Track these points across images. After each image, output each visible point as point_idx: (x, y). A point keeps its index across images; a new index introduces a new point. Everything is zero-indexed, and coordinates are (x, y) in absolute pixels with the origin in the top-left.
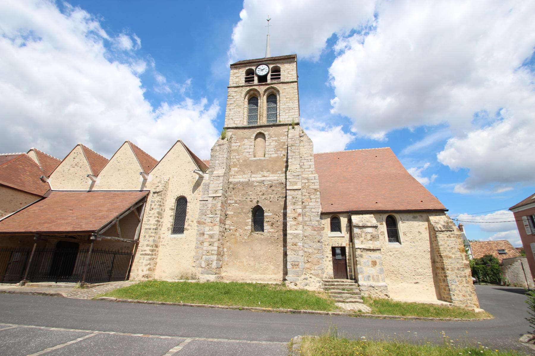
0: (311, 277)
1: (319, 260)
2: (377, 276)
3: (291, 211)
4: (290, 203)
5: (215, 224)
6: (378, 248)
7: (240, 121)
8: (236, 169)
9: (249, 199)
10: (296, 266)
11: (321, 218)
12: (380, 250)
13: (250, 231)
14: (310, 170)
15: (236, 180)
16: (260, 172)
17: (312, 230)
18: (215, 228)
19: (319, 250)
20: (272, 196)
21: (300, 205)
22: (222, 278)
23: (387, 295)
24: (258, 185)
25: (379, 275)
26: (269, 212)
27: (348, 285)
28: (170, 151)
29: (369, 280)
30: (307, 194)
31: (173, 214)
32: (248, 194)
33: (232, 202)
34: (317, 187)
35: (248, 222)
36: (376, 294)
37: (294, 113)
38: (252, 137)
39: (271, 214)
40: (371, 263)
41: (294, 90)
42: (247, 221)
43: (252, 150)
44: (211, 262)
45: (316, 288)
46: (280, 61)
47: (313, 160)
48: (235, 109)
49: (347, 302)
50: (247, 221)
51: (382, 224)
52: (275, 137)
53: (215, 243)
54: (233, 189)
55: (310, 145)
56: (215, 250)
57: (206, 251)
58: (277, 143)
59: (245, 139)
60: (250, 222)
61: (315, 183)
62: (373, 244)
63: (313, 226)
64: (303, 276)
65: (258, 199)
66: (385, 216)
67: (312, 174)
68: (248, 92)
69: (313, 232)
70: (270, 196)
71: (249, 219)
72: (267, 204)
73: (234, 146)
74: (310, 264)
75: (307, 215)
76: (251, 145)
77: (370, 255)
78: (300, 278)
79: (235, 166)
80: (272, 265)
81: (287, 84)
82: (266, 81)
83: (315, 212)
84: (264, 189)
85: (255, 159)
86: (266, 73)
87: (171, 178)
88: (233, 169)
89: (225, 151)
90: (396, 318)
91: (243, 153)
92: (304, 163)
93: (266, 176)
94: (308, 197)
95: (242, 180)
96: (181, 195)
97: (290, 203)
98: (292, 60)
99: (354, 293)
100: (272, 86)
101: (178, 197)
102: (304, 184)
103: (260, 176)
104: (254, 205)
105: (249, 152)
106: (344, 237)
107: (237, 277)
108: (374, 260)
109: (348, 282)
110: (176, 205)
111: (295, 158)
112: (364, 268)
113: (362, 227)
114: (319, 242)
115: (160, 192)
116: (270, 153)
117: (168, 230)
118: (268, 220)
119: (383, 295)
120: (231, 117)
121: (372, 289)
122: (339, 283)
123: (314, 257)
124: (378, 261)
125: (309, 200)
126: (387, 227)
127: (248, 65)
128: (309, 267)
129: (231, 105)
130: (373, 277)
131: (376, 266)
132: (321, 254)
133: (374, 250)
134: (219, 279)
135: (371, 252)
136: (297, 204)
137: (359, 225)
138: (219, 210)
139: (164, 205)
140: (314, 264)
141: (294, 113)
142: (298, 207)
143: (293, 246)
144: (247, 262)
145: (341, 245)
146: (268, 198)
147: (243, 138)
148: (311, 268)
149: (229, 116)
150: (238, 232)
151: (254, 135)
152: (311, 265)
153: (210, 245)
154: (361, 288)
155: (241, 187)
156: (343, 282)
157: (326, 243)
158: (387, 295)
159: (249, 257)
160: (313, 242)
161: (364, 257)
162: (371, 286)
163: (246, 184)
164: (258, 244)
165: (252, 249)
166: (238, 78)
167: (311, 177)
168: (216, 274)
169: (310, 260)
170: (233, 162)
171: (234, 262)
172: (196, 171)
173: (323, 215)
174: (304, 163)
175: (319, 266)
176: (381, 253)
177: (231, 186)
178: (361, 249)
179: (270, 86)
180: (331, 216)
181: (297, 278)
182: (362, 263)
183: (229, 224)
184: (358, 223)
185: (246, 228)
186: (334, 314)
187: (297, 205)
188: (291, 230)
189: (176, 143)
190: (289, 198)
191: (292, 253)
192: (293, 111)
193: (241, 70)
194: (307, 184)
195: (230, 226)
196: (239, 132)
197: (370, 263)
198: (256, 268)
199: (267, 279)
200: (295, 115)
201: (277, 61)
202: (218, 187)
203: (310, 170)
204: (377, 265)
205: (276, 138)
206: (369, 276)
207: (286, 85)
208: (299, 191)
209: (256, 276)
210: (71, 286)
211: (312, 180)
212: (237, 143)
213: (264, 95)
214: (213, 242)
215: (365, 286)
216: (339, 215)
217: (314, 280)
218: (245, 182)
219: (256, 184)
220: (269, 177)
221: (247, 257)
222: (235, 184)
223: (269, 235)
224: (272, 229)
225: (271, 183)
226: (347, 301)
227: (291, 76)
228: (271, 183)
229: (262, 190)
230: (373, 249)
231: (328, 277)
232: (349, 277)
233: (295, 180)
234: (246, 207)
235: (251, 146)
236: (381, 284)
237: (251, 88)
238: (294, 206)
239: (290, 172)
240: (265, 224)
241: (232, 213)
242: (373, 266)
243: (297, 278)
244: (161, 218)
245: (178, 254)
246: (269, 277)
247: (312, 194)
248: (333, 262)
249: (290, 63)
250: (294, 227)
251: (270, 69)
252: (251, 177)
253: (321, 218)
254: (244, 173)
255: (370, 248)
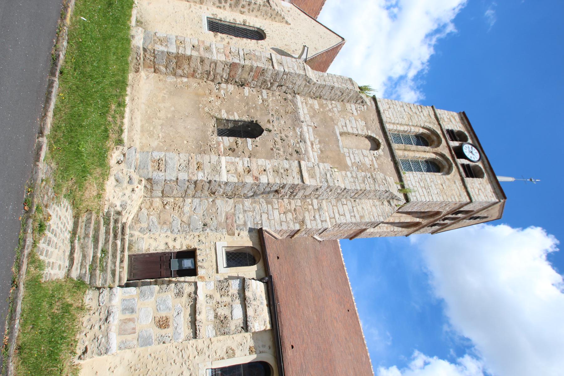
0: (133, 190)
1: (168, 223)
2: (134, 329)
3: (262, 166)
4: (277, 165)
5: (228, 57)
6: (198, 332)
7: (390, 118)
8: (317, 107)
9: (271, 119)
10: (157, 167)
11: (251, 230)
12: (195, 336)
13: (219, 117)
14: (337, 216)
15: (299, 105)
16: (318, 140)
17: (227, 213)
18: (221, 55)
19: (189, 225)
20: (282, 153)
21: (275, 180)
22: (137, 71)
23: (85, 352)
24: (296, 133)
25: (136, 335)
26: (254, 146)
27: (113, 268)
28: (327, 30)
29: (124, 310)
30: (293, 206)
31: (238, 22)
32: (281, 118)
33: (263, 95)
34: (309, 225)
35: (233, 114)
36: (89, 327)
37: (422, 194)
38: (369, 132)
39: (250, 148)
40: (164, 315)
41: (458, 197)
42: (235, 113)
43: (350, 130)
44: (164, 45)
45: (111, 198)
46: (492, 178)
47: (354, 220)
48: (404, 113)
49: (72, 242)
50: (235, 113)
51: (251, 352)
52: (378, 165)
53: (198, 53)
54: (285, 99)
55: (379, 216)
56: (185, 51)
57: (184, 41)
58: (369, 166)
59: (365, 122)
60: (234, 117)
61: (314, 222)
62: (207, 320)
63: (234, 214)
64: (136, 177)
65: (273, 131)
66: (268, 358)
67: (330, 218)
68: (434, 132)
69: (224, 215)
70: (282, 150)
71: (239, 117)
72: (268, 143)
73: (351, 106)
74: (161, 207)
75: (254, 205)
76: (357, 130)
77: (182, 315)
78: (132, 170)
79: (321, 106)
80: (158, 144)
81: (463, 187)
82: (459, 157)
83: (261, 220)
84: (292, 141)
85: (338, 135)
86: (469, 157)
87: (290, 26)
88: (316, 102)
89: (344, 85)
90: (12, 319)
91: (344, 118)
92: (346, 204)
93: (313, 148)
94: (289, 207)
95: (301, 111)
96: (267, 34)
97: (277, 165)
98: (500, 194)
99: (95, 269)
100: (454, 165)
101: (263, 31)
102: (310, 202)
103: (312, 139)
104: (263, 124)
105: (346, 126)
106: (217, 272)
107: (138, 92)
108: (170, 323)
109: (120, 272)
110: (251, 29)
111: (354, 182)
112: (153, 299)
113: (242, 295)
114: (204, 225)
115: (269, 5)
116: (352, 156)
117: (213, 15)
118: (240, 144)
119: (87, 343)
120: (392, 106)
121: (103, 317)
122: (119, 252)
123: (176, 215)
124: (169, 331)
125: (283, 210)
126: (244, 365)
127: (472, 133)
128: (154, 205)
129: (409, 109)
130: (130, 320)
131: (157, 328)
132: (180, 228)
133: (194, 322)
134: (135, 61)
135: (190, 315)
136: (276, 175)
137: (246, 289)
138: (251, 63)
139: (251, 11)
140: (159, 214)
141: (422, 194)
142: (270, 177)
143: (195, 163)
144: (164, 107)
145: (201, 267)
146: (277, 146)
147: (365, 119)
148: (152, 209)
149: (393, 104)
150: (216, 100)
151: (374, 135)
152: (157, 209)
153: (193, 46)
154: (106, 292)
155: (290, 108)
156: (122, 261)
157: (202, 238)
158: (85, 352)
159: (174, 111)
160: (204, 215)
161: (178, 300)
162: (109, 313)
163: (295, 116)
164: (196, 125)
165: (187, 116)
166: (449, 121)
167: (324, 215)
168: (145, 50)
169: (167, 207)
170: (326, 104)
171: (163, 89)
172: (306, 48)
173: (259, 234)
174: (346, 204)
175: (156, 223)
176: (188, 339)
177: (289, 97)
178: (195, 293)
179: (452, 161)
180: (258, 247)
181: (133, 166)
182: (163, 295)
183: (227, 88)
184: (250, 289)
185: (223, 111)
186: (40, 148)
187: (273, 176)
188: (227, 162)
189: (340, 37)
190: (285, 164)
191: (182, 161)
192: (426, 193)
193: (461, 125)
194: (310, 207)
195: (224, 89)
196: (373, 115)
197: (164, 314)
198: (154, 120)
199: (132, 134)
200: (420, 196)
201: (490, 173)
202: (288, 67)
203: (337, 216)
204: (159, 330)
205: (376, 166)
206: (133, 311)
207: (461, 184)
208: (300, 180)
209: (139, 119)
210: (124, 255)
211: (320, 215)
212: (357, 111)
213: (436, 153)
214: (198, 51)
215: (110, 300)
216: (261, 263)
217: (127, 195)
218: (299, 116)
219: (298, 130)
220: (313, 151)
221: (173, 109)
222: (292, 101)
223: (213, 143)
224: (225, 149)
225: (304, 152)
226: (76, 241)
227: (476, 193)
228: (304, 152)
229: (290, 138)
230: (195, 320)
231: (132, 241)
232: (129, 282)
233: (318, 175)
234: (258, 114)
235: (356, 130)
236: (115, 340)
237: (441, 136)
238: (271, 170)
239: (330, 169)
240: (232, 139)
241: (247, 94)
242: (157, 319)
243: (133, 166)
244: (231, 6)
245: (176, 21)
246: (137, 137)
247: (295, 216)
248: (164, 254)
249: (495, 192)
250: (232, 168)
251: (477, 164)
252: (308, 125)
253: (251, 230)
254: (311, 117)
255: (197, 315)
